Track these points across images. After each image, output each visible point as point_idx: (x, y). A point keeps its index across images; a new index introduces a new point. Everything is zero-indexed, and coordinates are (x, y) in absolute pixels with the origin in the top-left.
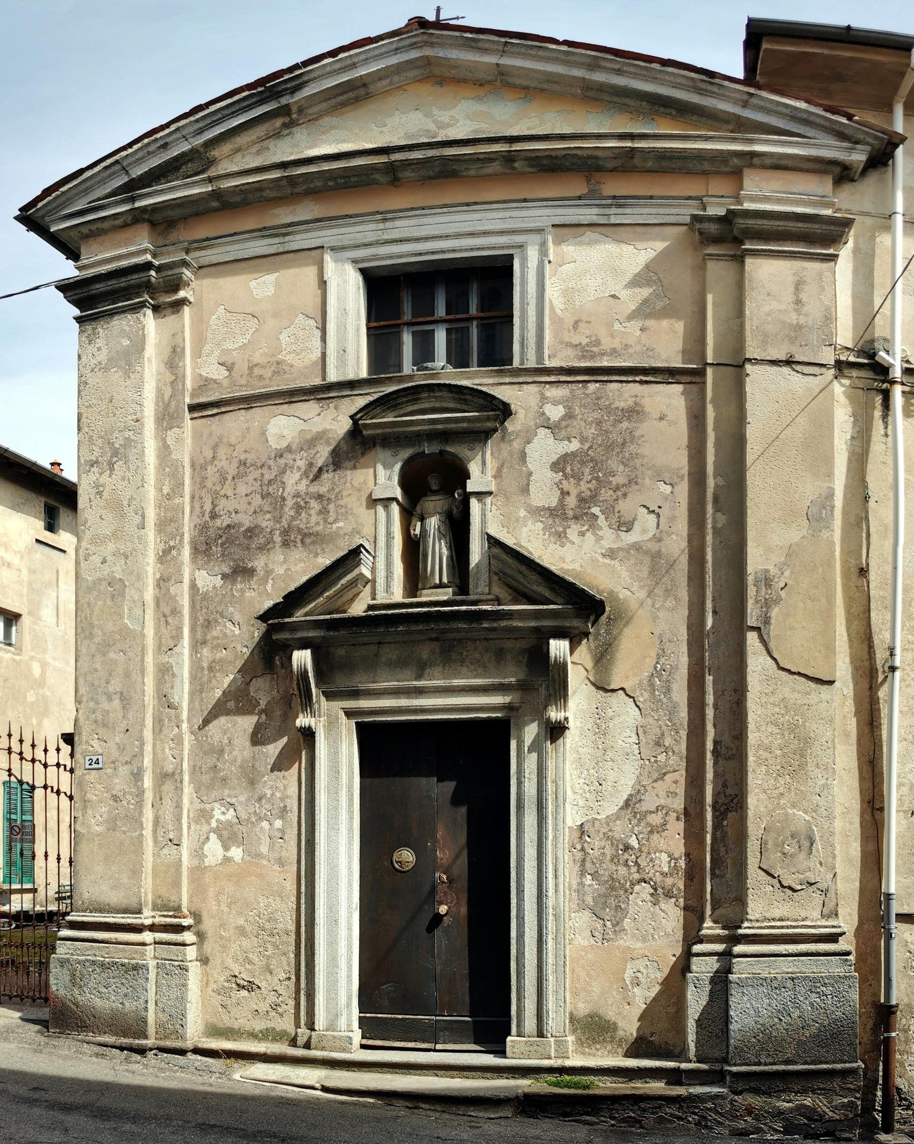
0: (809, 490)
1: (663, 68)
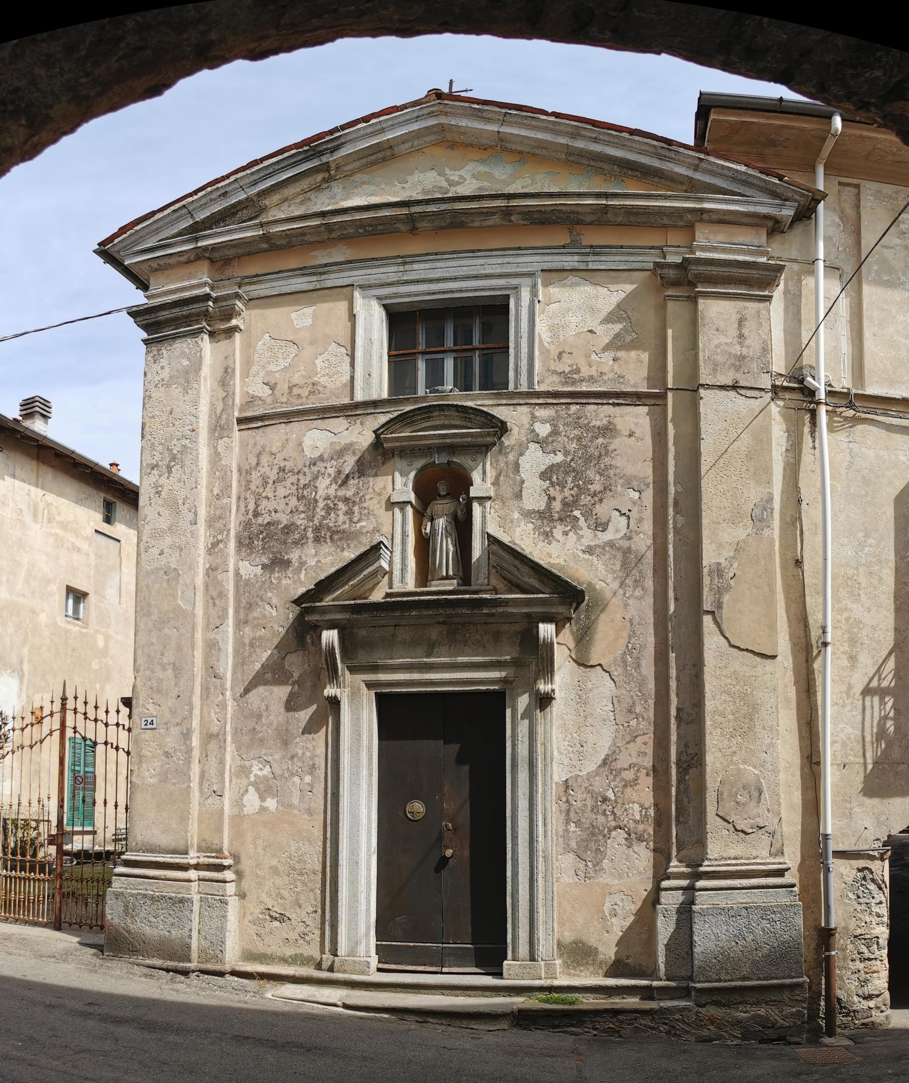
0: (753, 495)
1: (630, 137)
